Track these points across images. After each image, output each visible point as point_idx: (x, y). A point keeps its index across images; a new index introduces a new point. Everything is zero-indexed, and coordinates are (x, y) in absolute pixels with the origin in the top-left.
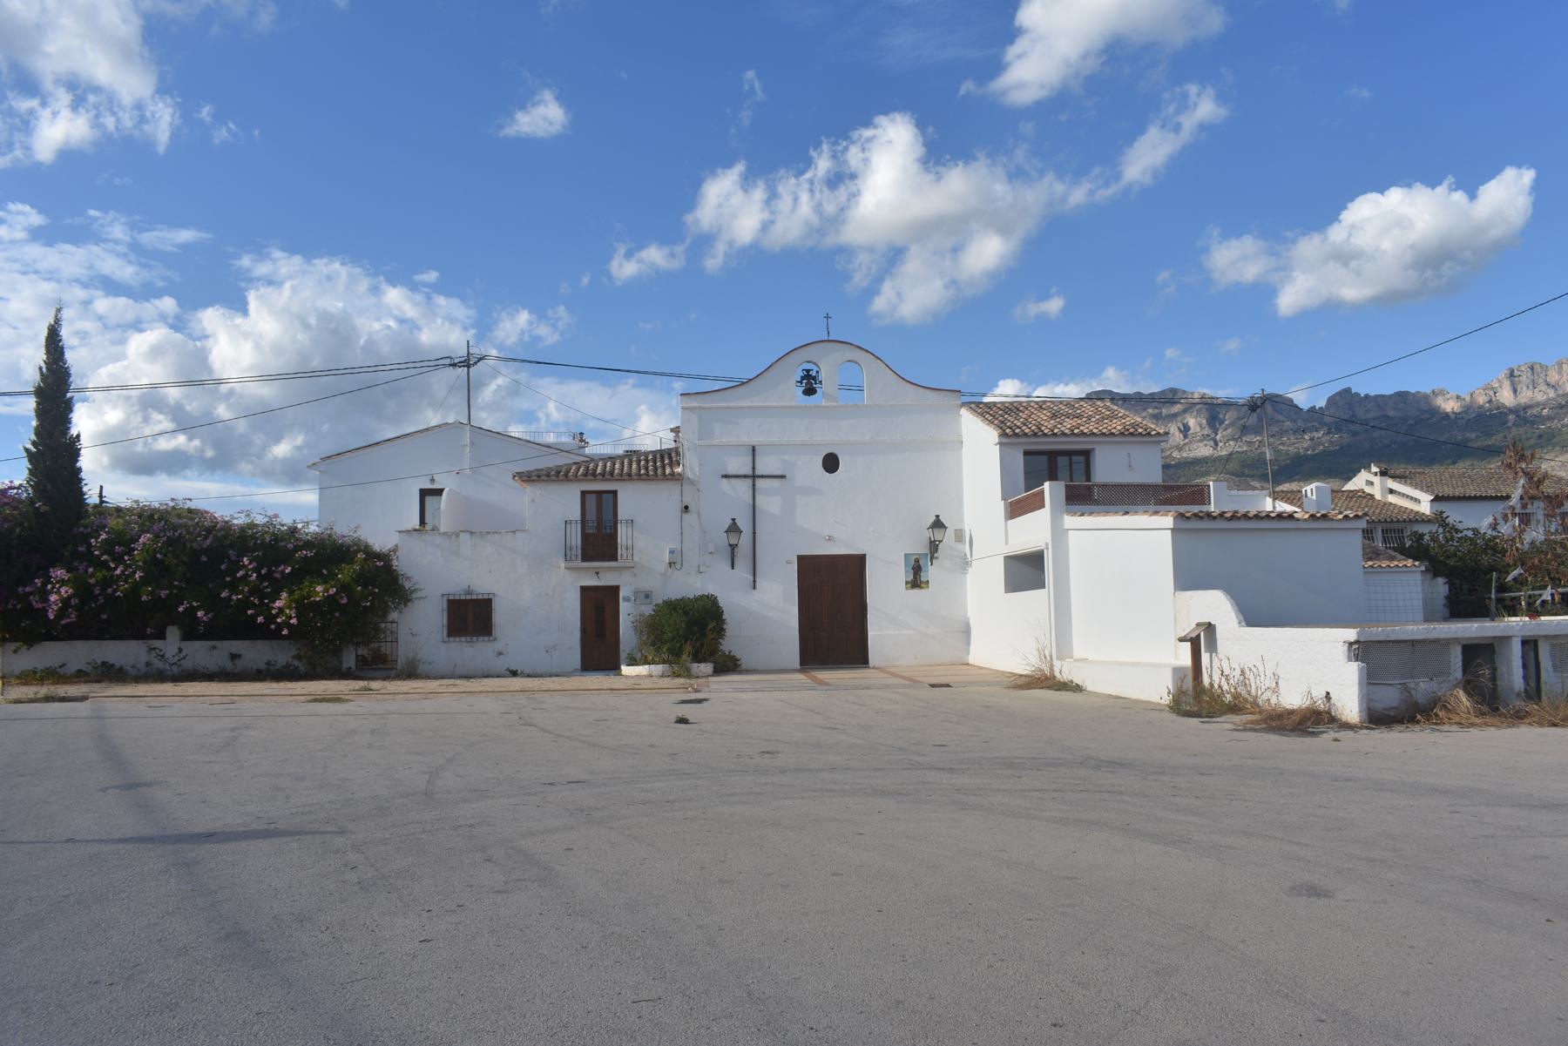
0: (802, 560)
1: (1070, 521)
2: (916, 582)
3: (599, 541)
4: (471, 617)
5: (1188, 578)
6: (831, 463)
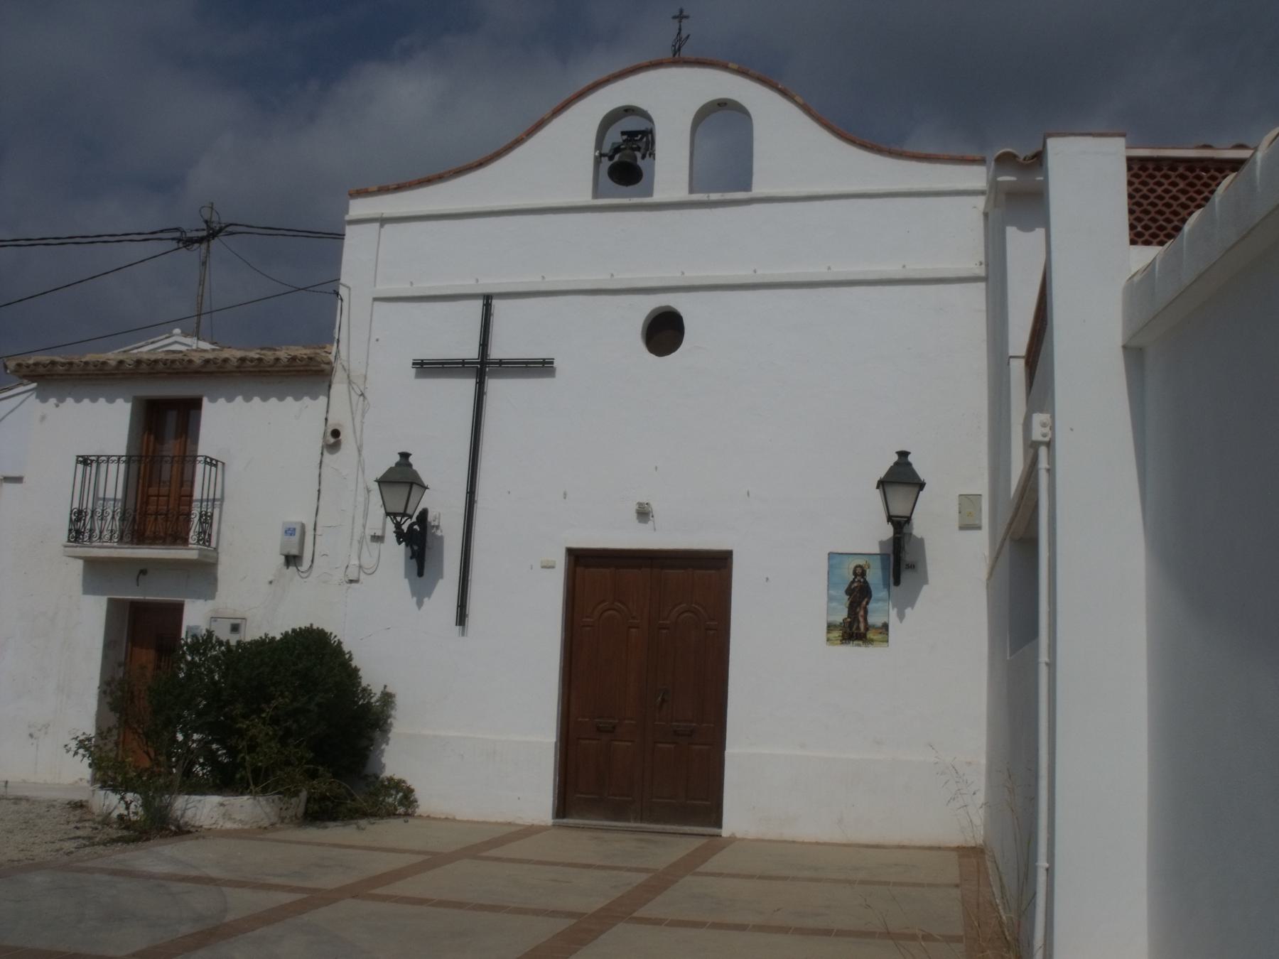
6: (664, 332)
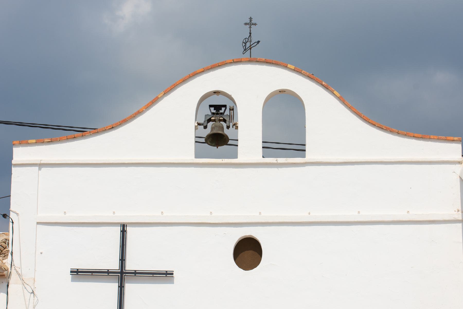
6: (248, 252)
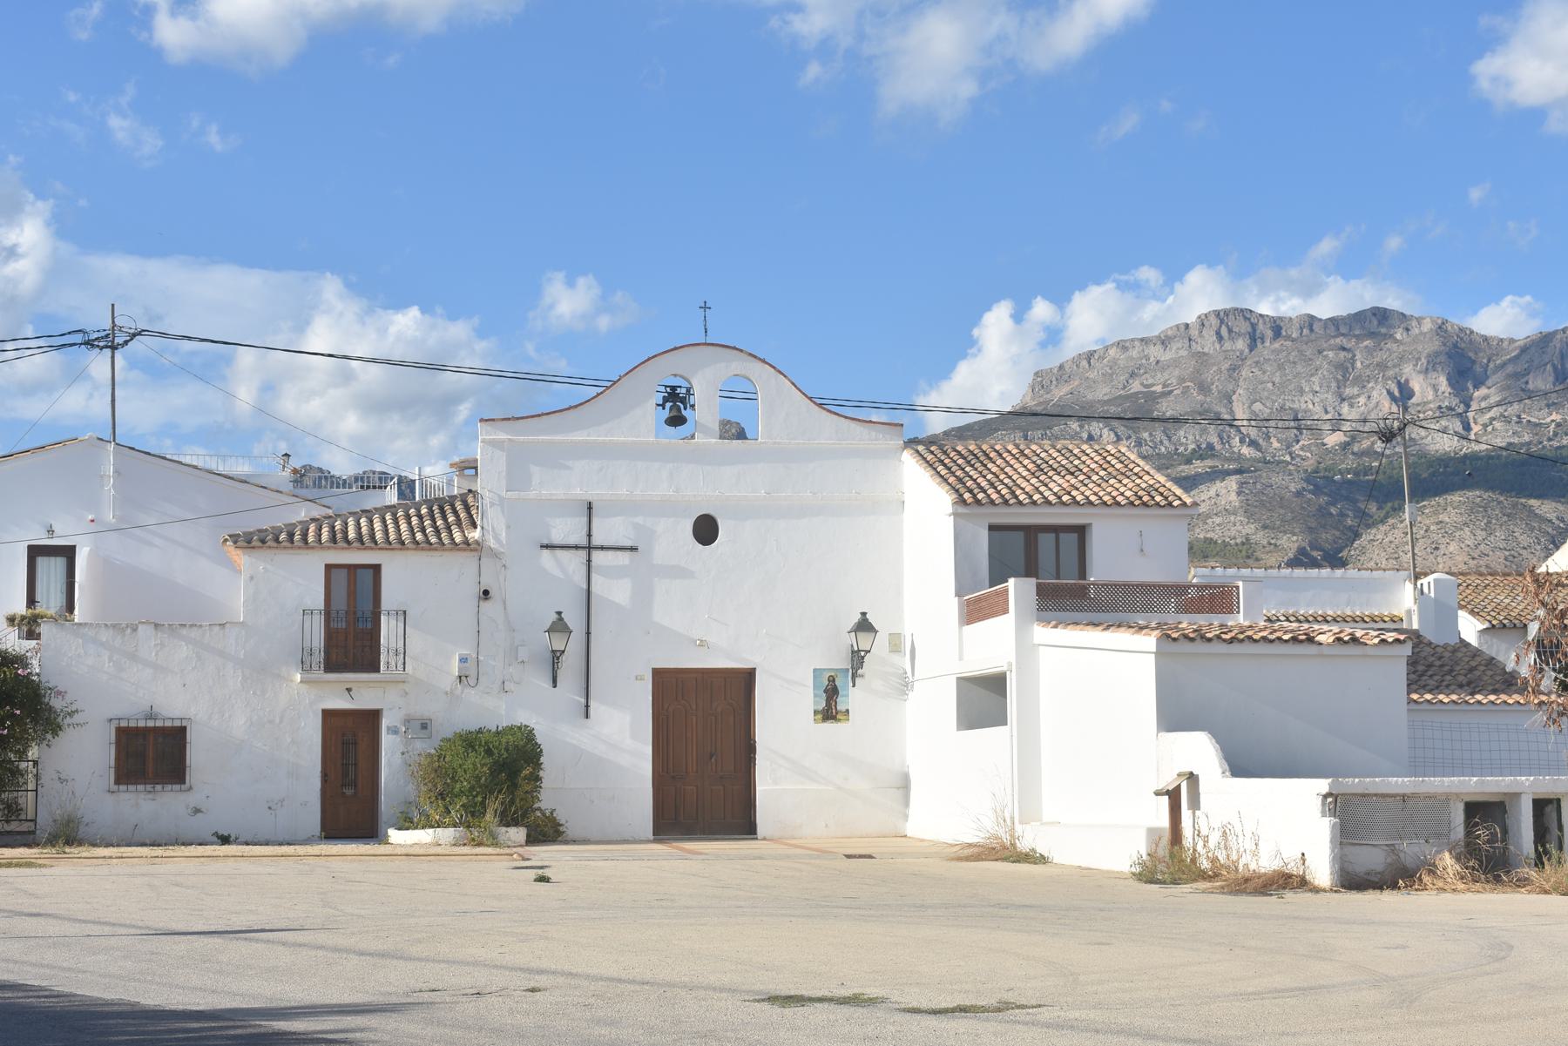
0: (660, 675)
1: (1043, 634)
2: (830, 712)
3: (351, 639)
4: (152, 754)
5: (1173, 717)
6: (706, 530)
